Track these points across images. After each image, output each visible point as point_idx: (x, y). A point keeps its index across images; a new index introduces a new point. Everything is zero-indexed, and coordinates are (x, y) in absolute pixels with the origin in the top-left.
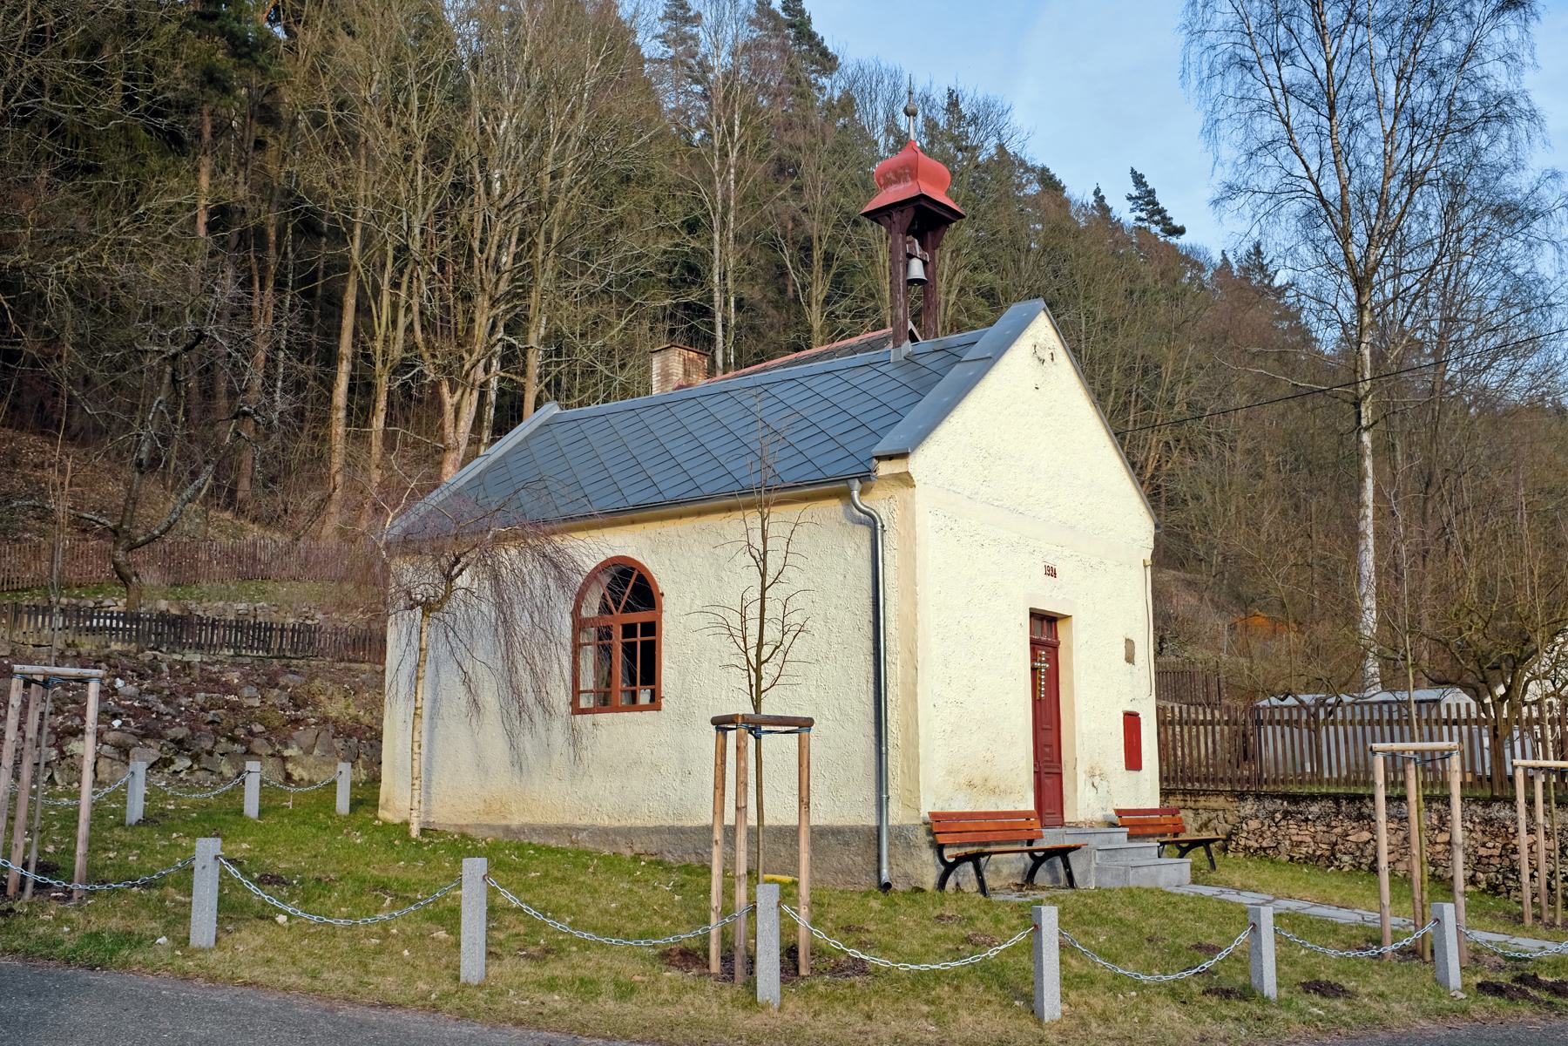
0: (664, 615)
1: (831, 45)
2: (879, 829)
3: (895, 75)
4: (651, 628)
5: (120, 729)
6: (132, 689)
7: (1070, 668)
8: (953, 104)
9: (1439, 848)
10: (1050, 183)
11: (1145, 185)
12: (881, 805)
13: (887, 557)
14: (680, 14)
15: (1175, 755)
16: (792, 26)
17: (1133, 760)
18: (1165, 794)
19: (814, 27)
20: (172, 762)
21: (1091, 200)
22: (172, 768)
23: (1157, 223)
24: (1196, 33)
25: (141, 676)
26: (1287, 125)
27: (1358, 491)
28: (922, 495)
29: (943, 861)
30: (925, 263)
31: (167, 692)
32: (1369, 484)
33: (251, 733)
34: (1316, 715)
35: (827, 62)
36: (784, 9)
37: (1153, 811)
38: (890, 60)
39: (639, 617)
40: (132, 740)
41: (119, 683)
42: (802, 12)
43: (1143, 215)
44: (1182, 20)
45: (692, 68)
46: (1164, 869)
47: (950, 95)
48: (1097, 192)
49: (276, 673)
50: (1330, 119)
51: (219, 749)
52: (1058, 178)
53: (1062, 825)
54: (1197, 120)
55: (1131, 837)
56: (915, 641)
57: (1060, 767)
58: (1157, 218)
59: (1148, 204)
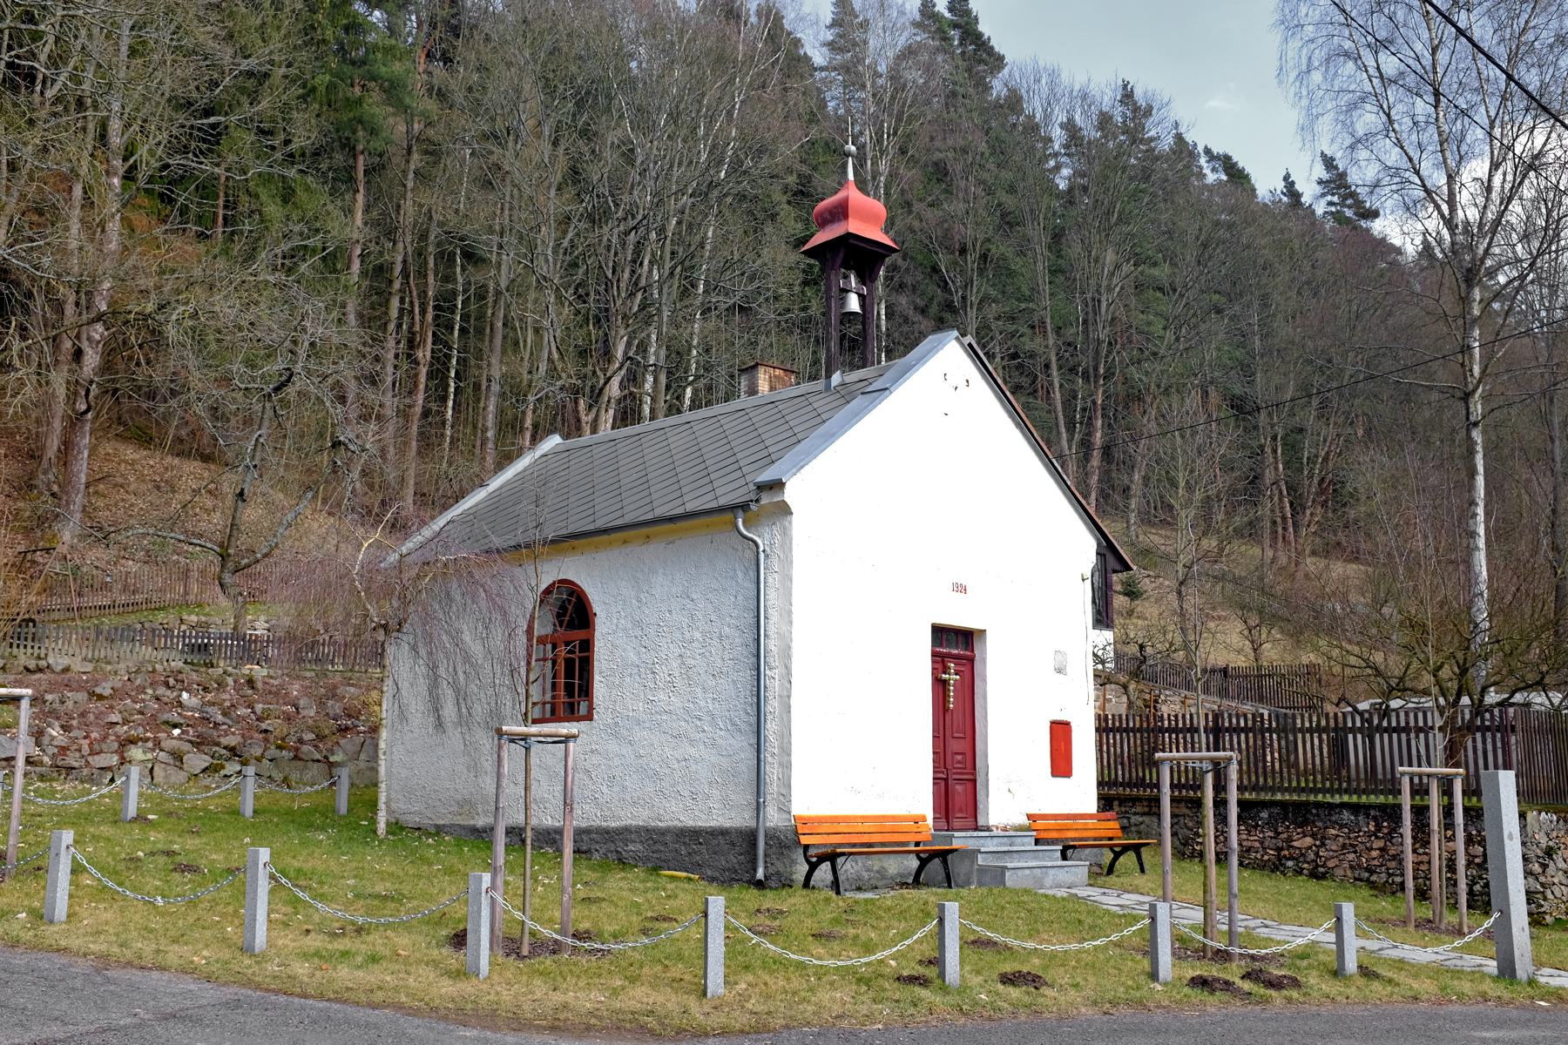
0: (597, 634)
1: (998, 45)
2: (757, 829)
3: (1054, 74)
4: (587, 646)
5: (179, 738)
6: (195, 701)
7: (984, 681)
8: (1127, 96)
9: (1375, 854)
10: (1236, 175)
11: (1336, 168)
12: (759, 808)
13: (770, 580)
14: (844, 18)
15: (1265, 761)
16: (956, 26)
17: (1061, 765)
18: (1105, 802)
19: (982, 27)
20: (223, 767)
21: (1280, 186)
22: (223, 772)
23: (1349, 207)
24: (1290, 25)
25: (205, 689)
26: (1388, 115)
27: (1472, 487)
28: (799, 523)
29: (808, 862)
30: (860, 295)
31: (228, 704)
32: (1480, 480)
33: (301, 741)
34: (1370, 721)
35: (998, 61)
36: (950, 10)
37: (1090, 816)
38: (1046, 60)
39: (580, 634)
40: (187, 747)
41: (185, 695)
42: (968, 12)
43: (1335, 199)
44: (1277, 16)
45: (852, 73)
46: (1052, 872)
47: (1125, 87)
48: (1286, 178)
49: (335, 687)
50: (1436, 107)
51: (268, 754)
52: (1241, 165)
53: (976, 829)
54: (1292, 117)
55: (1037, 842)
56: (789, 657)
57: (974, 774)
58: (1349, 202)
59: (1339, 187)
